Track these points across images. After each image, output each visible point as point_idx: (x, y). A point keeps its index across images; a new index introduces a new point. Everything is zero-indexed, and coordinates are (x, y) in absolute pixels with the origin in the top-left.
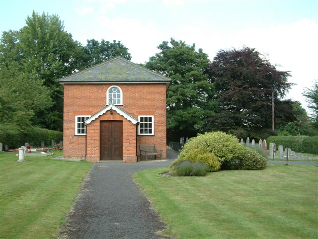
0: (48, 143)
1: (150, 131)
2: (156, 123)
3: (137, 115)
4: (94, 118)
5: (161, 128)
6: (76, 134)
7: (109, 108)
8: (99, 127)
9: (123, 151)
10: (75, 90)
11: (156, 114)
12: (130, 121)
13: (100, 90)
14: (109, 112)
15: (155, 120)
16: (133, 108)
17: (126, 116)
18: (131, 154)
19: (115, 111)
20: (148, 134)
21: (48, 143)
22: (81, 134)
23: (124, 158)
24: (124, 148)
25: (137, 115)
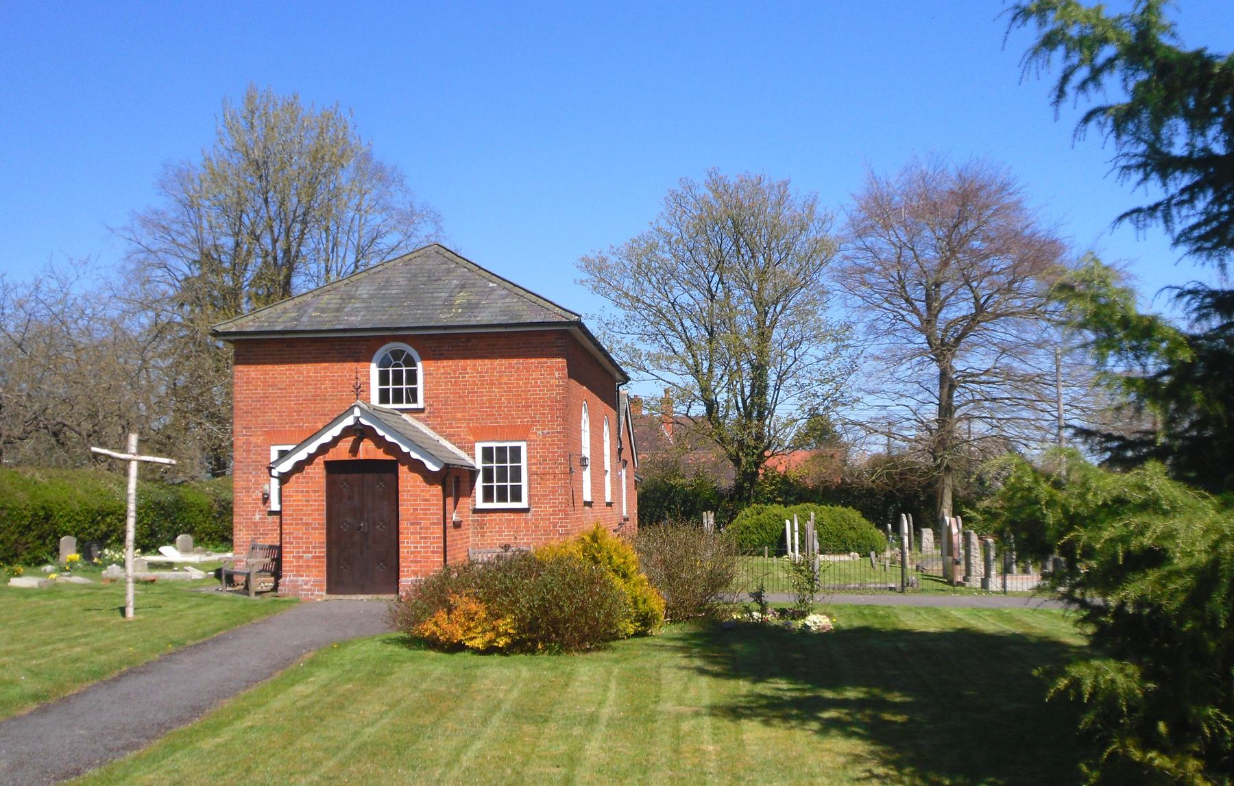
0: (715, 712)
1: (517, 497)
2: (534, 468)
3: (471, 438)
4: (302, 455)
5: (550, 484)
6: (480, 504)
8: (322, 482)
11: (534, 437)
15: (529, 458)
16: (459, 415)
20: (509, 505)
21: (715, 712)
22: (495, 505)
25: (471, 438)
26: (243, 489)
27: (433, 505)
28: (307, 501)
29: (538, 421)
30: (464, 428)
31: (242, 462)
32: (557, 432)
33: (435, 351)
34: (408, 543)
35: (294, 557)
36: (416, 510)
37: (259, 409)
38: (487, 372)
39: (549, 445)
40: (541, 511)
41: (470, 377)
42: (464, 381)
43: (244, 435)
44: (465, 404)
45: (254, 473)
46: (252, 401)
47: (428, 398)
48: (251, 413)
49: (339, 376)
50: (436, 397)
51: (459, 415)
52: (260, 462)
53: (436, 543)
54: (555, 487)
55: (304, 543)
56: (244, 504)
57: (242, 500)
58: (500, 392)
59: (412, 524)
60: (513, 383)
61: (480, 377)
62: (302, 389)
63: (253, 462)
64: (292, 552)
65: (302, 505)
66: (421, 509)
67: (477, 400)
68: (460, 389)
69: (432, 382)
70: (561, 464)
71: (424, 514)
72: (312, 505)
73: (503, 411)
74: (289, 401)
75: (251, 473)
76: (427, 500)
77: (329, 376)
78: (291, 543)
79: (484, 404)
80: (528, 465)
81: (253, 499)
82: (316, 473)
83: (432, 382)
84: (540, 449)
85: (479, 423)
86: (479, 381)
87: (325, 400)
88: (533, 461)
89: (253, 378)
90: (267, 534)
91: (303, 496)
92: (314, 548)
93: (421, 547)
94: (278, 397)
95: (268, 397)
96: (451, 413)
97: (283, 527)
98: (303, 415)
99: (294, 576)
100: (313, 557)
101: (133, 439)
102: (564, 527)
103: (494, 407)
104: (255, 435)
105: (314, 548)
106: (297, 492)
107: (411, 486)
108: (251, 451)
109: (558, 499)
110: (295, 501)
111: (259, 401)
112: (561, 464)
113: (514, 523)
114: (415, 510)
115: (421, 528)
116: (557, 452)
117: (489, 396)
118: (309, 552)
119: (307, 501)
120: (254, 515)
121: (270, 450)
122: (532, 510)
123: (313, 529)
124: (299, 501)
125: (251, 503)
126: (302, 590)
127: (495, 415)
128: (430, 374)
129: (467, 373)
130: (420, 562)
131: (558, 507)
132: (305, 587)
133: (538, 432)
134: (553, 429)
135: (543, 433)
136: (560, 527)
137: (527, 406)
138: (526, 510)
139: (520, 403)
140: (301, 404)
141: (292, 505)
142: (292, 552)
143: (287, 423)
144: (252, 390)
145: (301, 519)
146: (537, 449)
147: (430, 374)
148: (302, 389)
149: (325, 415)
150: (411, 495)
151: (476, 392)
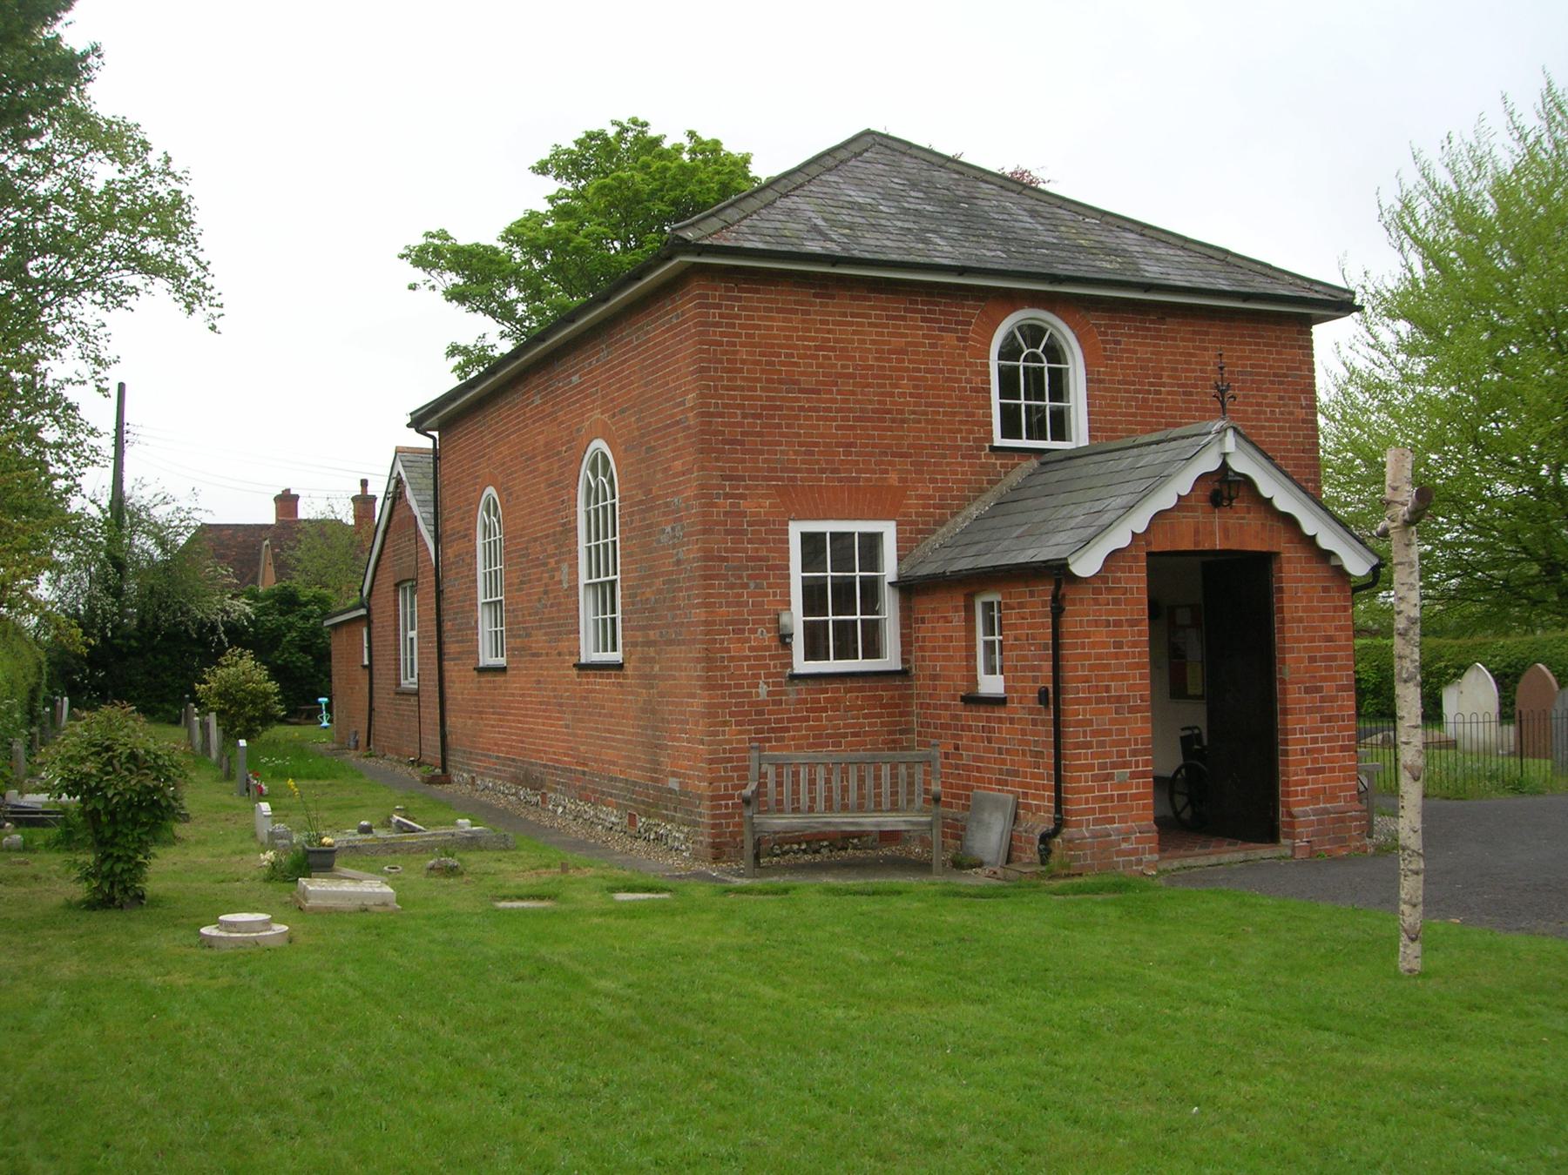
20: (859, 664)
26: (728, 623)
28: (1118, 645)
31: (725, 559)
33: (1105, 334)
35: (1095, 778)
37: (759, 434)
41: (1169, 393)
43: (727, 496)
45: (752, 585)
46: (745, 416)
48: (742, 443)
52: (766, 559)
56: (731, 659)
57: (728, 650)
62: (853, 393)
63: (749, 559)
64: (1090, 767)
69: (1104, 398)
74: (826, 419)
75: (746, 586)
78: (1087, 745)
81: (751, 649)
83: (1104, 398)
87: (903, 421)
89: (743, 362)
90: (787, 730)
92: (1134, 753)
94: (801, 409)
95: (780, 408)
99: (1097, 822)
106: (1096, 623)
110: (1093, 645)
111: (759, 416)
114: (1312, 659)
118: (1125, 765)
120: (757, 686)
124: (1104, 645)
125: (748, 658)
126: (1120, 853)
128: (1100, 381)
129: (1163, 385)
132: (1124, 846)
140: (852, 428)
141: (1087, 657)
142: (1090, 767)
144: (742, 389)
145: (1107, 689)
147: (1100, 381)
148: (853, 393)
149: (902, 455)
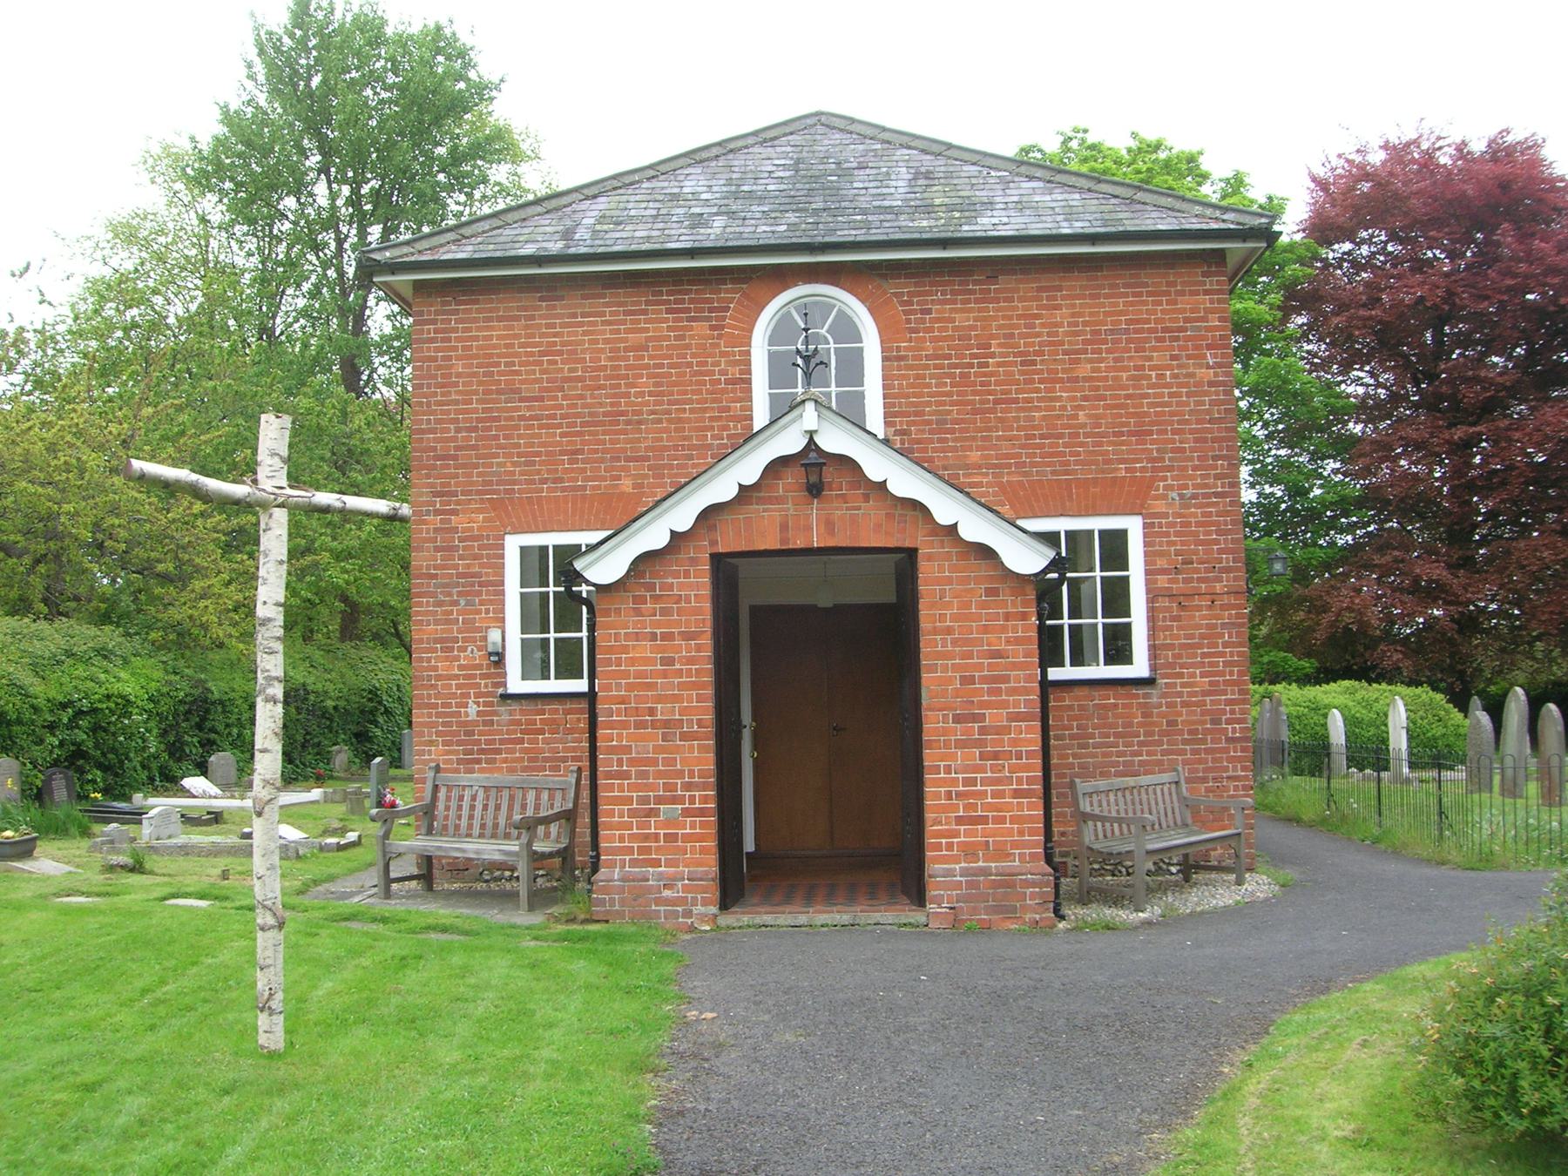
1: (1119, 650)
2: (1162, 581)
7: (789, 442)
9: (930, 828)
10: (497, 332)
11: (1159, 506)
12: (986, 553)
13: (701, 328)
14: (792, 479)
15: (1149, 556)
16: (975, 456)
17: (946, 507)
18: (1001, 854)
19: (847, 464)
20: (1102, 671)
23: (935, 868)
24: (934, 792)
26: (436, 641)
27: (1015, 666)
29: (1170, 469)
30: (989, 485)
31: (435, 576)
32: (1216, 495)
34: (948, 770)
36: (970, 680)
37: (473, 448)
38: (1040, 353)
39: (1198, 524)
40: (1183, 685)
41: (999, 365)
42: (985, 374)
43: (437, 512)
44: (989, 429)
45: (462, 602)
46: (458, 430)
47: (895, 415)
48: (455, 458)
49: (671, 366)
50: (916, 414)
51: (975, 456)
53: (1027, 768)
54: (1214, 626)
55: (659, 774)
56: (439, 678)
57: (435, 669)
58: (1074, 399)
59: (957, 719)
60: (1106, 379)
61: (1023, 363)
63: (460, 575)
65: (653, 674)
66: (984, 680)
67: (1017, 419)
68: (975, 393)
69: (904, 377)
70: (1227, 570)
71: (991, 692)
72: (679, 673)
73: (1082, 445)
75: (456, 603)
76: (998, 654)
77: (647, 367)
78: (624, 775)
79: (1033, 428)
80: (1147, 572)
81: (461, 667)
82: (691, 586)
83: (904, 377)
84: (1177, 534)
85: (1025, 474)
86: (1022, 373)
87: (639, 422)
88: (1161, 563)
89: (459, 375)
90: (498, 751)
91: (654, 649)
92: (688, 786)
93: (984, 782)
94: (522, 418)
96: (955, 449)
97: (600, 732)
98: (584, 461)
100: (687, 813)
101: (273, 434)
102: (1239, 721)
103: (1061, 436)
104: (465, 511)
105: (688, 786)
106: (637, 637)
107: (954, 618)
108: (455, 548)
109: (1222, 654)
110: (632, 661)
111: (475, 429)
112: (1227, 570)
113: (1116, 716)
115: (983, 731)
116: (1216, 542)
117: (1048, 409)
118: (675, 800)
119: (669, 661)
121: (502, 547)
122: (1162, 681)
123: (684, 736)
124: (647, 661)
125: (457, 677)
127: (1062, 454)
129: (992, 355)
130: (983, 820)
131: (1222, 674)
132: (667, 893)
133: (1166, 501)
134: (1206, 486)
135: (1182, 496)
136: (1228, 722)
137: (1140, 434)
138: (1148, 682)
139: (1123, 425)
141: (626, 674)
143: (544, 481)
144: (456, 402)
145: (652, 712)
146: (1167, 534)
150: (954, 642)
151: (1016, 401)
